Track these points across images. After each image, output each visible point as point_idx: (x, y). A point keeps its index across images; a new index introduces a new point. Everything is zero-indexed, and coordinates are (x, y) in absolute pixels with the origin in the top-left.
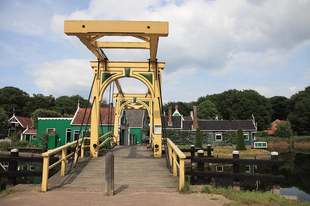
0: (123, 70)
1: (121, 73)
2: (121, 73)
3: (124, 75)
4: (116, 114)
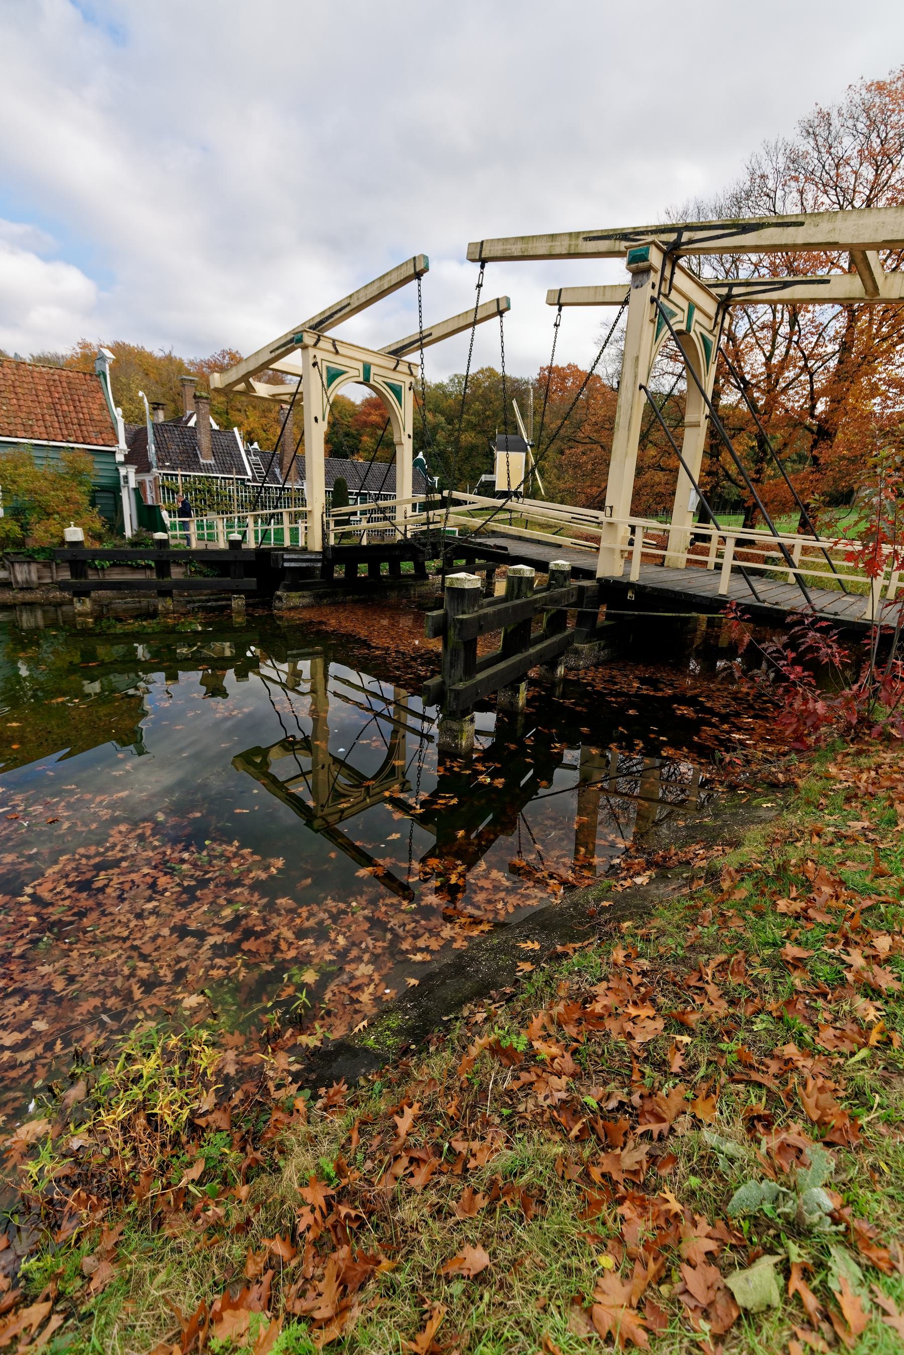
0: (360, 366)
1: (356, 373)
2: (356, 373)
3: (361, 379)
4: (316, 420)
